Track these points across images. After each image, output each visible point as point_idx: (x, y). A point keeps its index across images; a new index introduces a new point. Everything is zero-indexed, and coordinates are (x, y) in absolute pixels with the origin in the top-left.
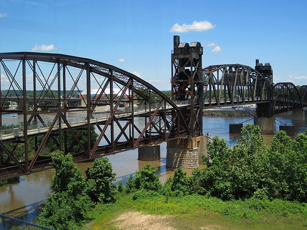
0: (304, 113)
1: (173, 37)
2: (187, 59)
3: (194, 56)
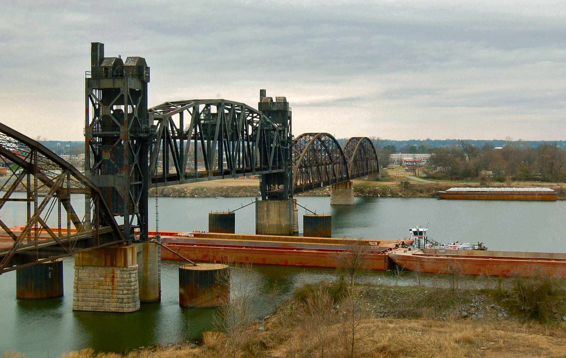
0: (353, 189)
1: (90, 46)
2: (118, 90)
3: (134, 84)
